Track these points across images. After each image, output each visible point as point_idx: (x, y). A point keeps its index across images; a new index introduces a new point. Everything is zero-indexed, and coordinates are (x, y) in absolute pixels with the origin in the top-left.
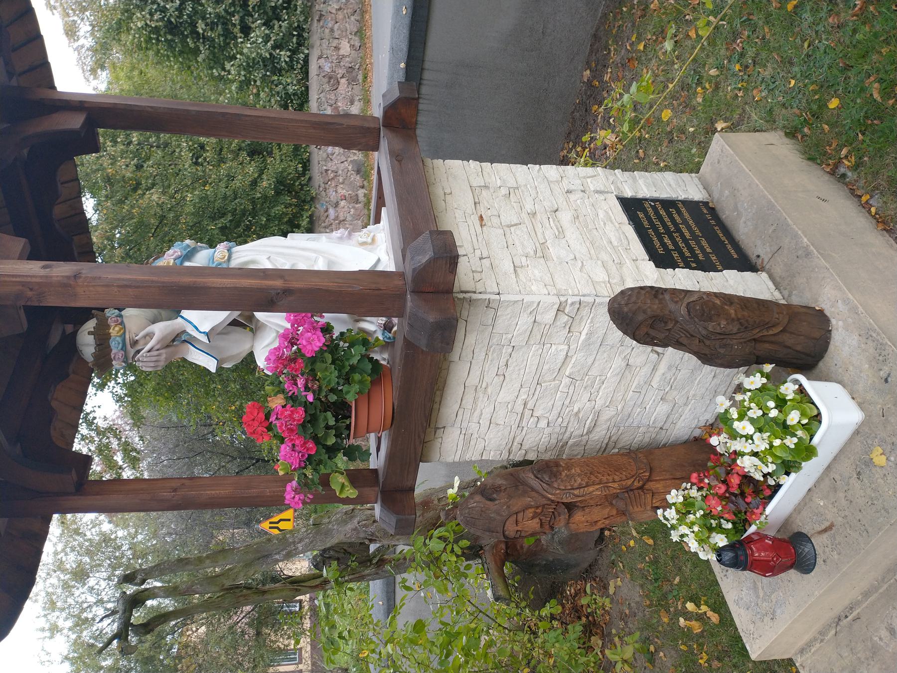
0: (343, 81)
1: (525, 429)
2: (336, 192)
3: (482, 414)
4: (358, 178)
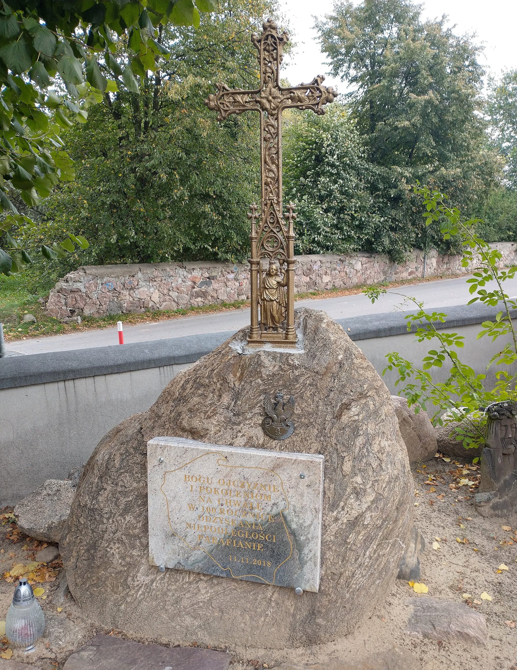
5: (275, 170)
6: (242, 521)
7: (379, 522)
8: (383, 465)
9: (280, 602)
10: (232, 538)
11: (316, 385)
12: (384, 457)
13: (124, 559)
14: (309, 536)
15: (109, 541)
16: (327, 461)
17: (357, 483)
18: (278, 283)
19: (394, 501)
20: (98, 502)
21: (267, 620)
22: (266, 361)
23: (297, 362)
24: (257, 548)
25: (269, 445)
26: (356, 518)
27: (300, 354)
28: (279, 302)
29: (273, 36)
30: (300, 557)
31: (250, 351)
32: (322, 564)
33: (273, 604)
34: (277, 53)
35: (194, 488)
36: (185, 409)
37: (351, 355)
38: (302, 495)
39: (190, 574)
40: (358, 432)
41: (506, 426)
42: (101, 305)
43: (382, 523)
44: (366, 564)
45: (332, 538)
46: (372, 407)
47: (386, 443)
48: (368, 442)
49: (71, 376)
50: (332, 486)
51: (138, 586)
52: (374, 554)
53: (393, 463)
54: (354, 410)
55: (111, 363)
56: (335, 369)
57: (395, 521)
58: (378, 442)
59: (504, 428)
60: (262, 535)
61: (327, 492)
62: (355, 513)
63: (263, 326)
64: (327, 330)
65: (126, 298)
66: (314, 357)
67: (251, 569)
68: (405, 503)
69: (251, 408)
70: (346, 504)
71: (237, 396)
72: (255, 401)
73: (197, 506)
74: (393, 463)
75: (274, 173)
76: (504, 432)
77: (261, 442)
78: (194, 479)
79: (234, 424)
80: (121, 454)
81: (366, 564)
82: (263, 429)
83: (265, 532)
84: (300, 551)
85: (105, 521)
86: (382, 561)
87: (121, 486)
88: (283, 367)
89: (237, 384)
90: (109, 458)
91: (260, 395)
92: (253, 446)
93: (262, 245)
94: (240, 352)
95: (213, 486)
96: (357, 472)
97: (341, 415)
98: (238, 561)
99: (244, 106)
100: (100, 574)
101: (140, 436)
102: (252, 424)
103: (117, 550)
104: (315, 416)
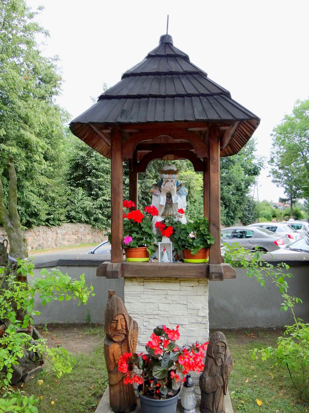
0: (76, 237)
1: (143, 317)
2: (30, 236)
3: (152, 298)
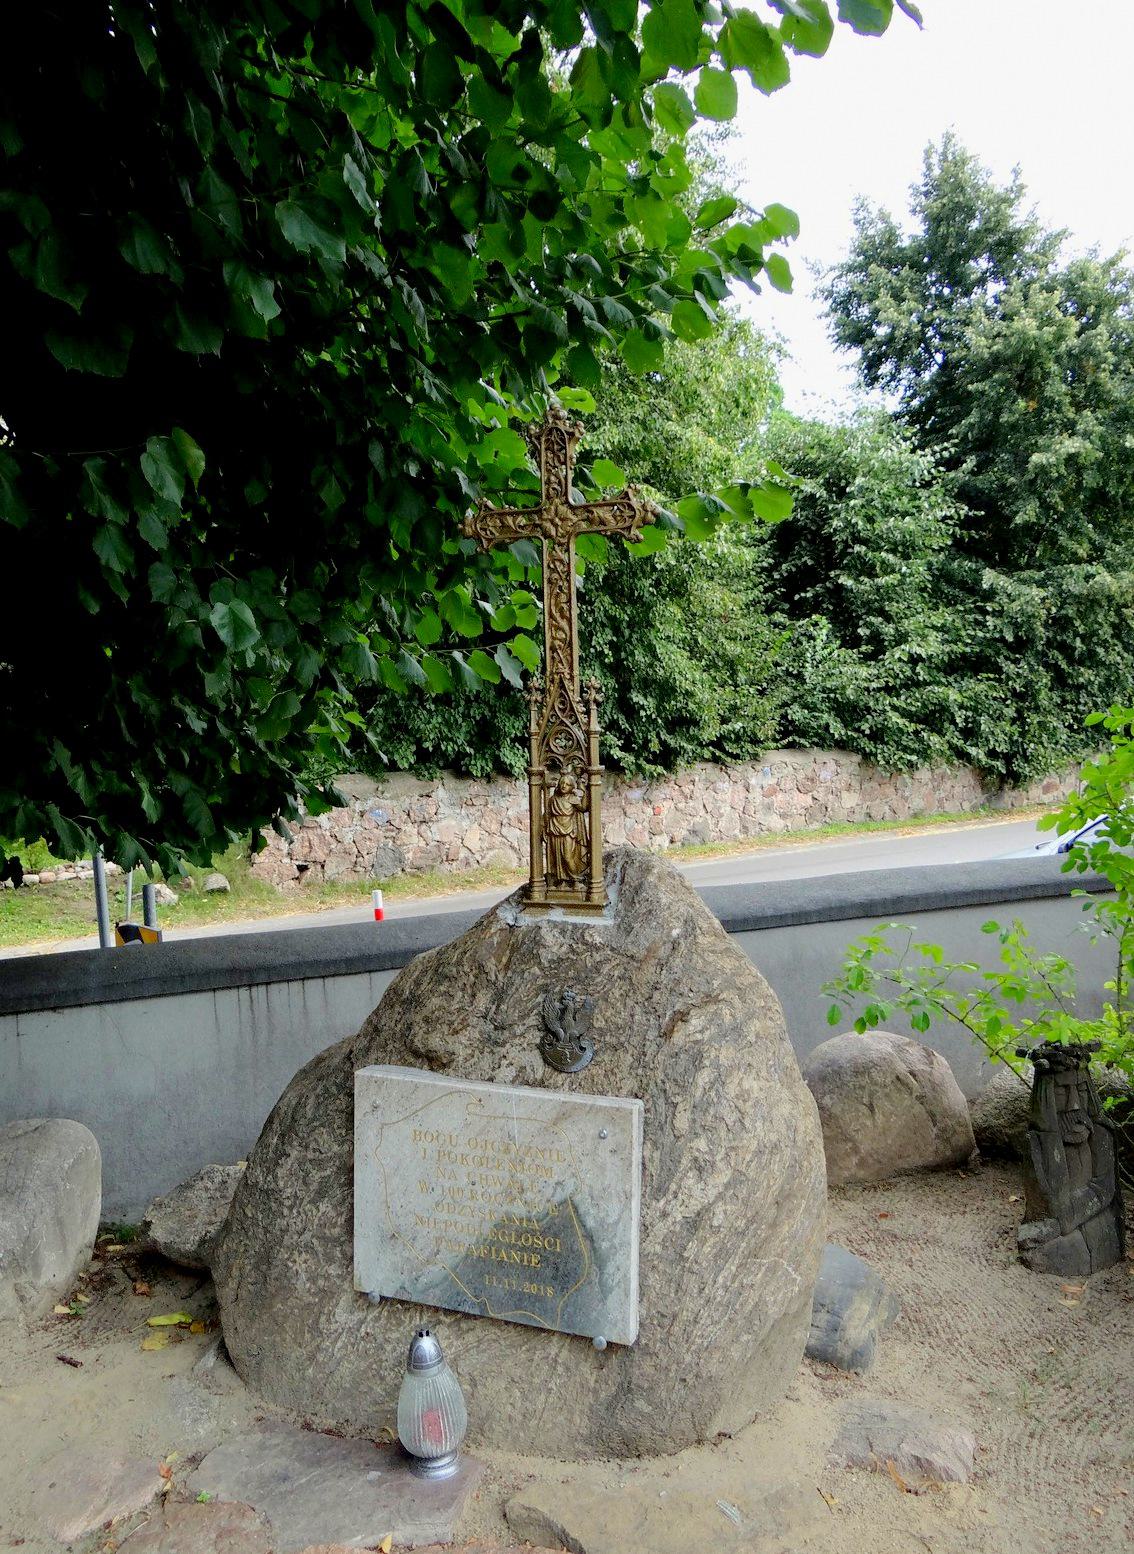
4: (684, 833)
5: (567, 628)
6: (506, 1213)
7: (741, 1224)
8: (747, 1123)
9: (572, 1365)
10: (492, 1244)
11: (631, 979)
12: (748, 1107)
13: (314, 1283)
14: (616, 1241)
15: (291, 1249)
16: (647, 1111)
17: (698, 1150)
18: (574, 806)
19: (769, 1187)
20: (275, 1178)
21: (551, 1400)
22: (549, 937)
23: (598, 940)
24: (530, 1262)
25: (552, 1081)
26: (698, 1214)
27: (606, 927)
28: (576, 838)
29: (558, 430)
30: (600, 1280)
31: (527, 920)
32: (642, 1295)
33: (560, 1369)
34: (565, 455)
35: (428, 1152)
36: (418, 1018)
37: (693, 929)
38: (602, 1168)
39: (422, 1311)
40: (701, 1062)
41: (1067, 1087)
42: (359, 854)
43: (747, 1228)
44: (719, 1299)
45: (658, 1248)
46: (728, 1019)
47: (755, 1085)
48: (719, 1081)
49: (262, 977)
50: (657, 1155)
51: (336, 1331)
52: (733, 1282)
53: (768, 1119)
54: (696, 1022)
55: (336, 955)
56: (663, 952)
57: (774, 1225)
58: (736, 1081)
59: (1062, 1091)
60: (538, 1238)
61: (647, 1163)
62: (695, 1205)
63: (552, 879)
64: (656, 886)
65: (413, 841)
66: (629, 931)
67: (520, 1300)
68: (795, 1196)
69: (522, 1018)
70: (680, 1187)
71: (499, 997)
72: (530, 1005)
73: (434, 1185)
74: (768, 1119)
75: (564, 631)
76: (1063, 1099)
77: (539, 1076)
78: (429, 1138)
79: (496, 1043)
80: (318, 1096)
81: (719, 1299)
82: (543, 1053)
83: (544, 1233)
84: (601, 1268)
85: (286, 1212)
86: (748, 1297)
87: (314, 1150)
88: (575, 946)
89: (500, 977)
90: (299, 1103)
91: (537, 995)
92: (527, 1084)
93: (548, 744)
94: (512, 923)
95: (460, 1150)
96: (700, 1131)
97: (672, 1031)
98: (500, 1286)
99: (516, 532)
100: (275, 1310)
101: (348, 1064)
102: (525, 1045)
103: (304, 1266)
104: (628, 1032)
